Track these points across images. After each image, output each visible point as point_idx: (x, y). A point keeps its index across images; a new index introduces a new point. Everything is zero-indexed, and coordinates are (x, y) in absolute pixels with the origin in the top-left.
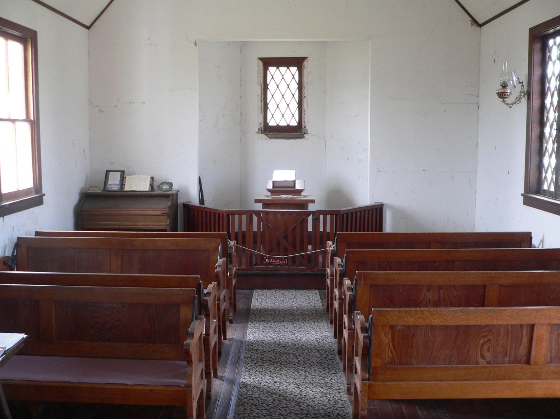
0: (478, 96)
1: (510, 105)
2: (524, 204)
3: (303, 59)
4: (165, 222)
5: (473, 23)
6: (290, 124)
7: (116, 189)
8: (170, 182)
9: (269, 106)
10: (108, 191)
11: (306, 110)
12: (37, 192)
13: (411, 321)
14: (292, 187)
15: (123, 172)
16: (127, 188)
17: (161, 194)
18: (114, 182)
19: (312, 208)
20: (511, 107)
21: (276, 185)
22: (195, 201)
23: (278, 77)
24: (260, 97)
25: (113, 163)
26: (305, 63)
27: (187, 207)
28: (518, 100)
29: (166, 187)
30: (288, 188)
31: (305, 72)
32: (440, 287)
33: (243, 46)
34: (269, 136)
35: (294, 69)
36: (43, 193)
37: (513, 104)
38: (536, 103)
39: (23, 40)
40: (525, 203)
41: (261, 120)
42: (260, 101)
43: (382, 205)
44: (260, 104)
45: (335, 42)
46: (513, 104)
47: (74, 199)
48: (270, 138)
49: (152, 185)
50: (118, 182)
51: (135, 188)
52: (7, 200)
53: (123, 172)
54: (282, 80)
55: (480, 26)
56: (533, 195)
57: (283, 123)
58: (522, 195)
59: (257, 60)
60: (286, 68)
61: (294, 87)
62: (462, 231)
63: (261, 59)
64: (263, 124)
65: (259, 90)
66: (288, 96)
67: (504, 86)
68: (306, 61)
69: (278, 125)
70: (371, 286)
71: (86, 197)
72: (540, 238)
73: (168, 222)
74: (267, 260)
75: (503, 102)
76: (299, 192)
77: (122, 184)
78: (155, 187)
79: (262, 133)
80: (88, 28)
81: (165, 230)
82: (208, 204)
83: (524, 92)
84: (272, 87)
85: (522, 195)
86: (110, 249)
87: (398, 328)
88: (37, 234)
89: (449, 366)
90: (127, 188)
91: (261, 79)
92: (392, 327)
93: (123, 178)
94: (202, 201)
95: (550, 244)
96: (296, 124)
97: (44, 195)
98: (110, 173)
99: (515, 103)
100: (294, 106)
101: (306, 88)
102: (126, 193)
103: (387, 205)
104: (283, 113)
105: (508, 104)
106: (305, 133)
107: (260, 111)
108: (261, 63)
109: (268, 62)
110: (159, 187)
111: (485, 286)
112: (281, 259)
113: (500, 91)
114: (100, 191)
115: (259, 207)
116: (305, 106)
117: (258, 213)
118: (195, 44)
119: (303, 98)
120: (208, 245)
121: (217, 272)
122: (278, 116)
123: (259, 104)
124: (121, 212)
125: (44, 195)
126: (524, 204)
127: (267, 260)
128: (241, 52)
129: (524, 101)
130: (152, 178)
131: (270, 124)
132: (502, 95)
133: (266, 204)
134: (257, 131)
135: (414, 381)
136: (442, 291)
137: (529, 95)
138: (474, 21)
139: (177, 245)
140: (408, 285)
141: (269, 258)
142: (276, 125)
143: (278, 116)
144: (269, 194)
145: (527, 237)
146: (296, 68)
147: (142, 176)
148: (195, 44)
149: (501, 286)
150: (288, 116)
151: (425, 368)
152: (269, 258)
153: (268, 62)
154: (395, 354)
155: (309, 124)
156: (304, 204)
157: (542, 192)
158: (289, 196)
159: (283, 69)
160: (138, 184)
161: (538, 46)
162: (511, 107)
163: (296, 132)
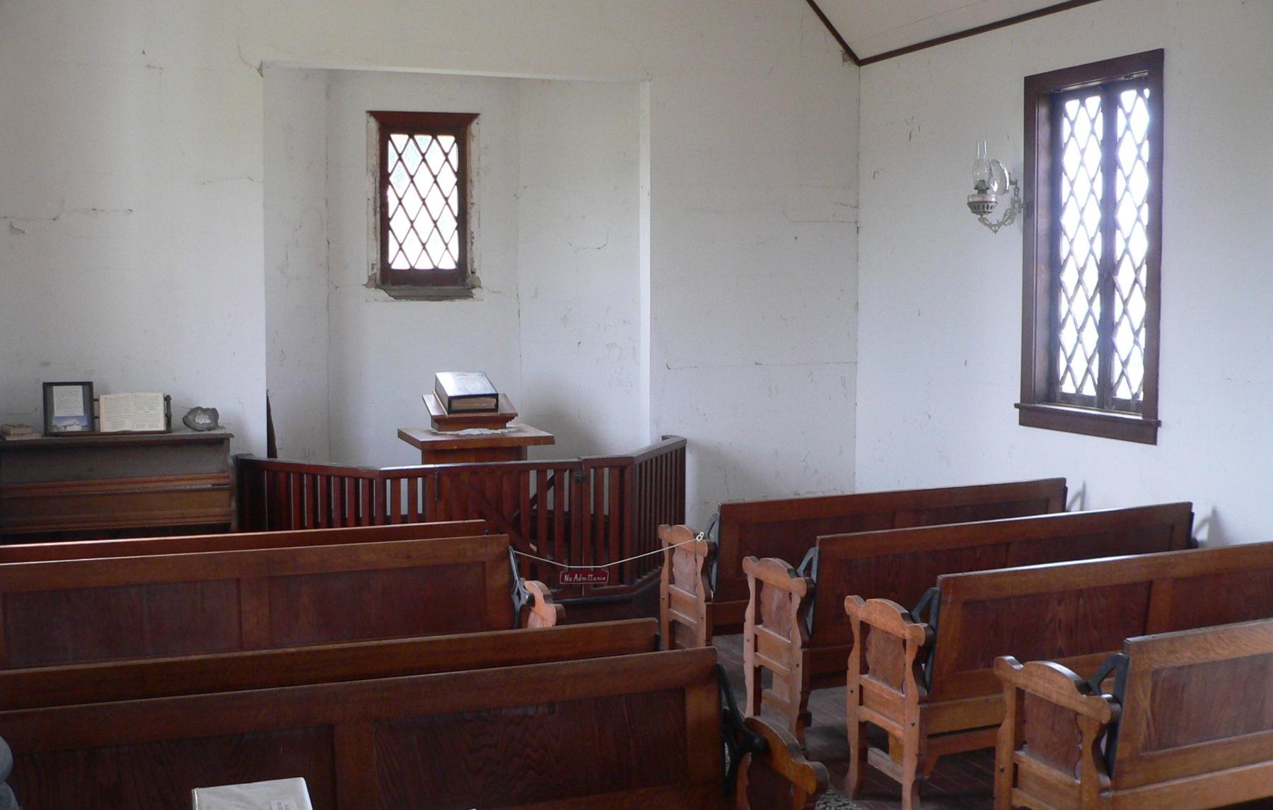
0: (857, 207)
1: (995, 228)
2: (1022, 423)
3: (470, 118)
4: (224, 507)
5: (846, 57)
6: (441, 267)
7: (77, 428)
8: (211, 407)
9: (392, 224)
10: (57, 435)
13: (1186, 657)
14: (492, 410)
15: (88, 386)
17: (193, 439)
18: (69, 412)
19: (534, 456)
20: (996, 231)
21: (455, 405)
22: (261, 453)
23: (412, 157)
24: (372, 201)
25: (47, 364)
26: (474, 127)
27: (247, 467)
28: (1009, 216)
29: (203, 420)
31: (474, 147)
32: (1079, 593)
33: (333, 80)
34: (393, 293)
35: (448, 141)
37: (999, 225)
38: (1042, 223)
40: (1023, 422)
41: (375, 256)
42: (371, 212)
43: (685, 441)
44: (372, 220)
45: (543, 81)
46: (999, 225)
48: (397, 298)
49: (168, 418)
50: (81, 412)
54: (423, 167)
55: (860, 63)
56: (1042, 406)
57: (424, 264)
58: (1016, 406)
59: (364, 116)
60: (406, 137)
61: (449, 181)
62: (820, 495)
63: (376, 115)
64: (379, 266)
65: (369, 185)
66: (435, 202)
67: (982, 188)
68: (476, 121)
69: (412, 270)
70: (965, 604)
72: (1079, 487)
73: (234, 505)
75: (982, 220)
78: (177, 420)
79: (377, 287)
81: (225, 528)
82: (282, 457)
83: (1019, 201)
84: (398, 178)
85: (1016, 406)
86: (238, 581)
87: (1164, 674)
89: (1233, 738)
90: (106, 426)
91: (375, 161)
92: (1156, 673)
93: (91, 401)
95: (1100, 503)
96: (452, 266)
98: (55, 388)
99: (1003, 223)
100: (449, 225)
101: (476, 183)
104: (424, 240)
105: (990, 226)
106: (473, 287)
107: (372, 236)
108: (373, 124)
109: (392, 122)
110: (186, 421)
111: (1151, 583)
113: (977, 199)
114: (36, 437)
115: (413, 461)
116: (473, 225)
117: (412, 475)
120: (483, 551)
123: (367, 219)
124: (107, 488)
126: (1022, 423)
127: (566, 578)
128: (327, 96)
129: (1019, 221)
130: (167, 399)
131: (394, 267)
132: (979, 207)
133: (431, 451)
134: (365, 281)
135: (1182, 777)
136: (1081, 601)
137: (1029, 210)
138: (849, 53)
139: (409, 557)
140: (1026, 596)
141: (572, 573)
143: (412, 247)
145: (1055, 491)
146: (451, 139)
147: (142, 394)
148: (260, 70)
149: (1177, 580)
150: (435, 246)
151: (1197, 748)
152: (572, 573)
153: (392, 122)
154: (1152, 729)
155: (482, 267)
156: (517, 448)
157: (1059, 397)
158: (486, 432)
159: (423, 140)
160: (145, 418)
161: (1042, 112)
162: (996, 231)
163: (452, 284)
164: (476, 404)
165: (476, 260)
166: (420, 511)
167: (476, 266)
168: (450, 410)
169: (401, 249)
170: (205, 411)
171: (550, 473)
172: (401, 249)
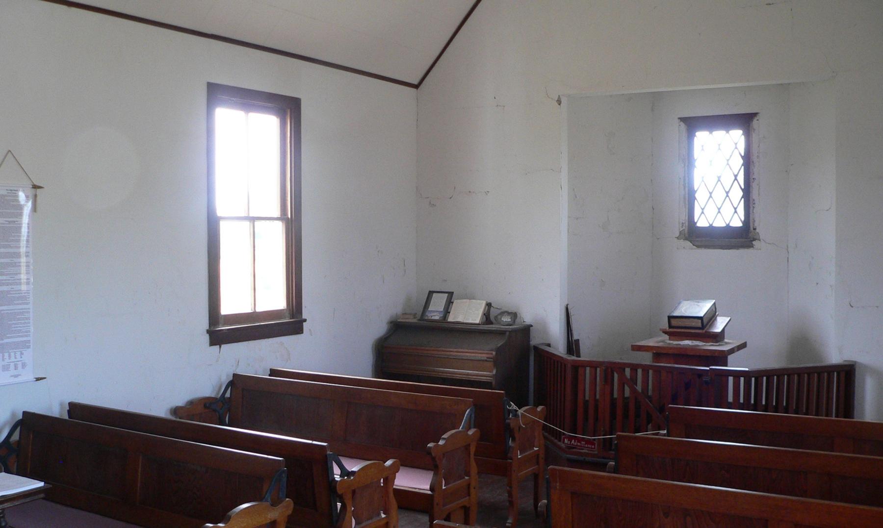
7: (437, 318)
11: (757, 202)
12: (292, 316)
15: (451, 294)
16: (451, 319)
19: (735, 365)
21: (674, 322)
29: (506, 319)
30: (701, 328)
36: (304, 317)
39: (281, 114)
47: (379, 329)
48: (698, 247)
51: (460, 319)
52: (225, 324)
53: (451, 294)
69: (711, 225)
71: (397, 327)
73: (494, 372)
74: (566, 441)
76: (718, 338)
77: (447, 312)
79: (686, 239)
80: (416, 87)
88: (273, 372)
90: (451, 319)
93: (449, 302)
94: (573, 346)
97: (305, 320)
102: (452, 326)
103: (866, 367)
106: (754, 240)
110: (496, 317)
112: (588, 442)
114: (415, 321)
115: (646, 359)
116: (755, 194)
117: (646, 369)
118: (559, 102)
119: (752, 180)
121: (430, 448)
122: (711, 211)
125: (305, 320)
127: (566, 441)
128: (652, 110)
130: (489, 305)
131: (699, 225)
133: (659, 354)
134: (677, 235)
141: (570, 438)
142: (707, 225)
143: (711, 211)
144: (667, 337)
148: (559, 102)
152: (570, 438)
155: (762, 227)
156: (722, 358)
160: (469, 313)
164: (688, 323)
165: (757, 220)
166: (742, 401)
167: (756, 224)
168: (670, 326)
169: (735, 209)
170: (509, 313)
171: (628, 371)
172: (735, 209)
